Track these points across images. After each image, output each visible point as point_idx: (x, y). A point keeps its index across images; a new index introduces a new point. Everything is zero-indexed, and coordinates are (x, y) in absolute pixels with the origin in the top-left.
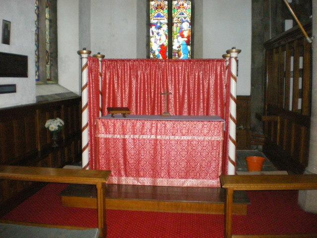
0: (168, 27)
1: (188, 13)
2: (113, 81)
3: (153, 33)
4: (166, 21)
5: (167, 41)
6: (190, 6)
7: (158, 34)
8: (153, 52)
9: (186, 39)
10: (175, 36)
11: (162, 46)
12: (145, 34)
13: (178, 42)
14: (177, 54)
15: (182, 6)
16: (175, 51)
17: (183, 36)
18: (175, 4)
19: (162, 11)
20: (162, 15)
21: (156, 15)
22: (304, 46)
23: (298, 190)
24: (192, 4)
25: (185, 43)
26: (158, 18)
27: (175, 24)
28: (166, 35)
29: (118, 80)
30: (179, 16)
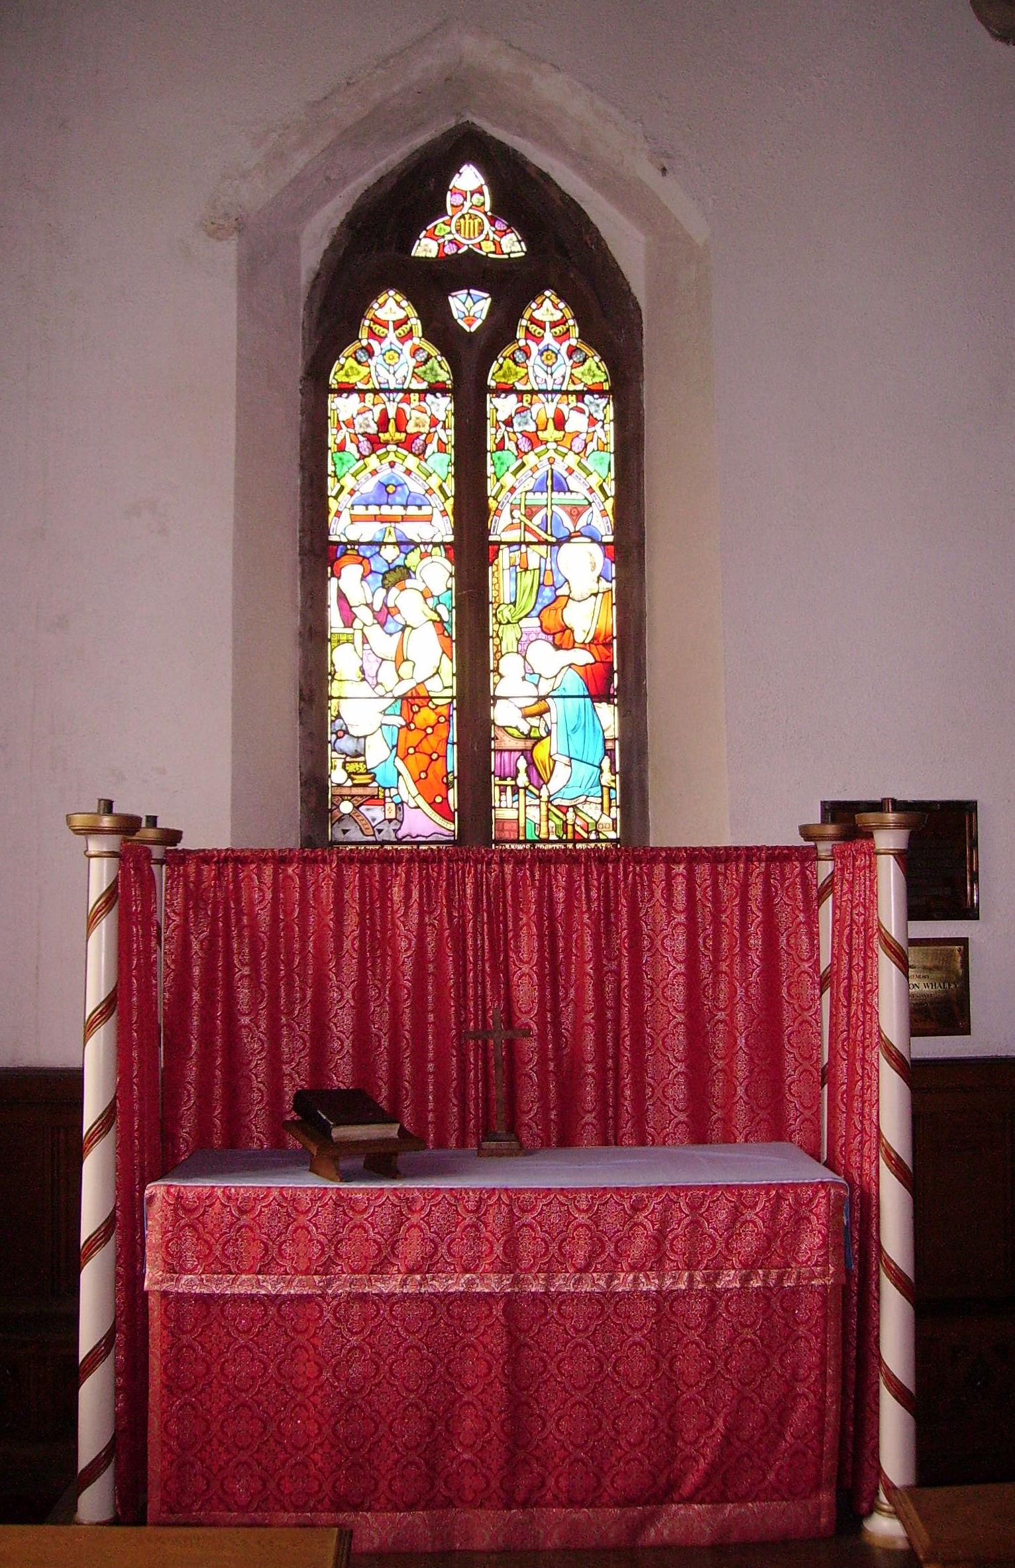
0: (458, 575)
1: (594, 481)
2: (229, 968)
3: (349, 618)
4: (443, 529)
5: (449, 668)
6: (607, 433)
7: (383, 616)
8: (346, 744)
9: (584, 657)
10: (509, 635)
11: (413, 701)
12: (291, 622)
13: (529, 672)
14: (522, 764)
15: (392, 434)
16: (509, 743)
17: (561, 637)
18: (502, 416)
19: (412, 462)
20: (415, 486)
21: (368, 486)
22: (544, 689)
23: (115, 1522)
24: (621, 421)
25: (574, 684)
26: (385, 510)
27: (505, 556)
28: (439, 623)
29: (254, 963)
30: (539, 499)
